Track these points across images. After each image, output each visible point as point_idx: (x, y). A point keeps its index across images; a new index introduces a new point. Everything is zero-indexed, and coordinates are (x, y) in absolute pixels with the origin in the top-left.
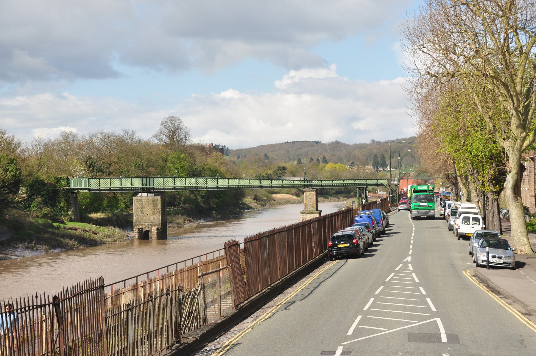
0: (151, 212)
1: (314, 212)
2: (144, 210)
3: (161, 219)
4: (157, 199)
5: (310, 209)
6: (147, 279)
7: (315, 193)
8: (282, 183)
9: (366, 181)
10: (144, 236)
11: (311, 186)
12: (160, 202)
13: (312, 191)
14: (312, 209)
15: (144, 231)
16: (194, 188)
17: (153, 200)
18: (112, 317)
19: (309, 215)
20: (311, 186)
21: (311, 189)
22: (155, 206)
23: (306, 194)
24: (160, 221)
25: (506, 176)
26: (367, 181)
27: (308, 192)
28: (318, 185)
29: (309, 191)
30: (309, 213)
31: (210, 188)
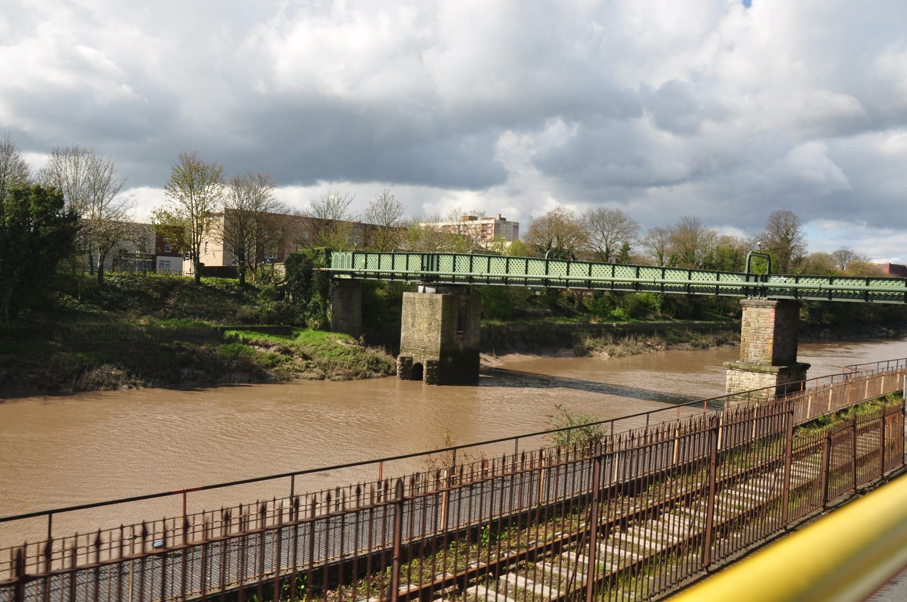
0: (426, 325)
1: (763, 369)
2: (417, 320)
3: (440, 342)
4: (437, 300)
5: (757, 359)
6: (46, 535)
7: (773, 314)
8: (690, 278)
9: (797, 282)
10: (412, 372)
11: (764, 291)
12: (441, 306)
13: (764, 306)
14: (762, 360)
15: (414, 363)
16: (539, 281)
17: (432, 302)
18: (740, 425)
19: (750, 375)
20: (764, 291)
21: (764, 300)
22: (433, 314)
23: (747, 314)
24: (439, 346)
25: (739, 315)
26: (872, 283)
27: (754, 309)
28: (814, 293)
29: (758, 306)
30: (748, 371)
31: (671, 289)
